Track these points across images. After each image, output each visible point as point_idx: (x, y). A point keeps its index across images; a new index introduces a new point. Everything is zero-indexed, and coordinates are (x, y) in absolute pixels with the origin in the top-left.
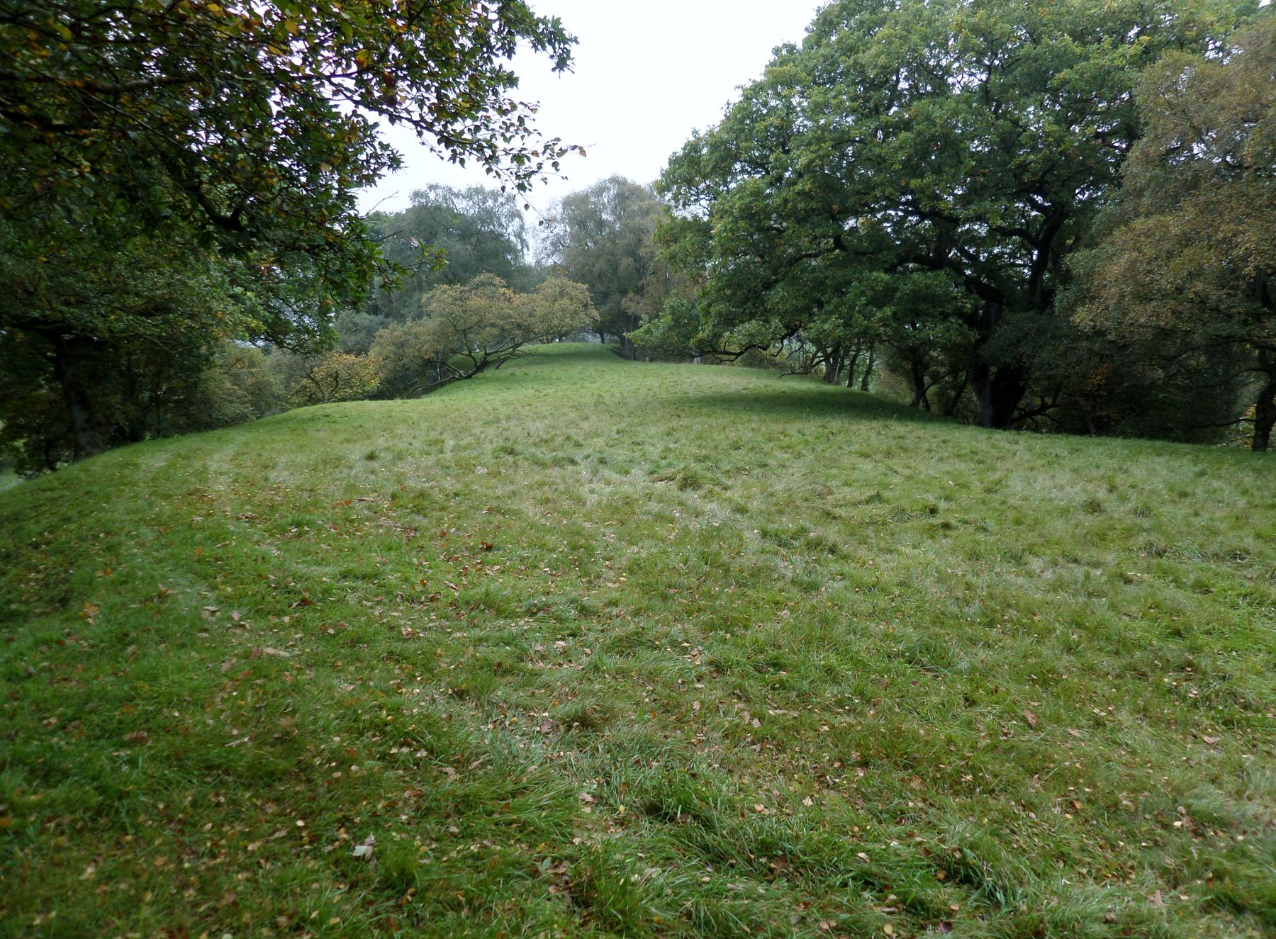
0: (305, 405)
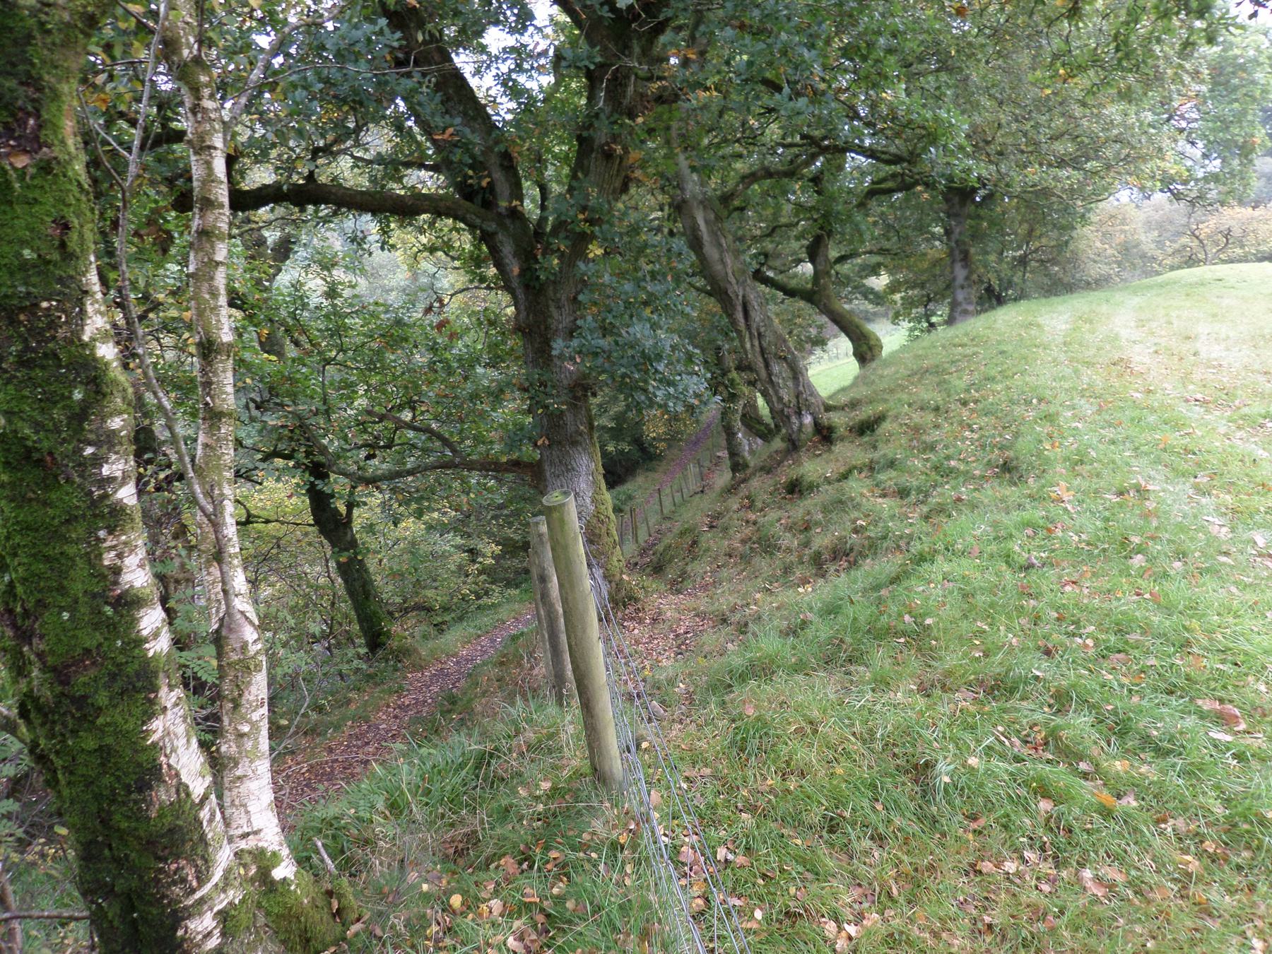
0: (1179, 268)
